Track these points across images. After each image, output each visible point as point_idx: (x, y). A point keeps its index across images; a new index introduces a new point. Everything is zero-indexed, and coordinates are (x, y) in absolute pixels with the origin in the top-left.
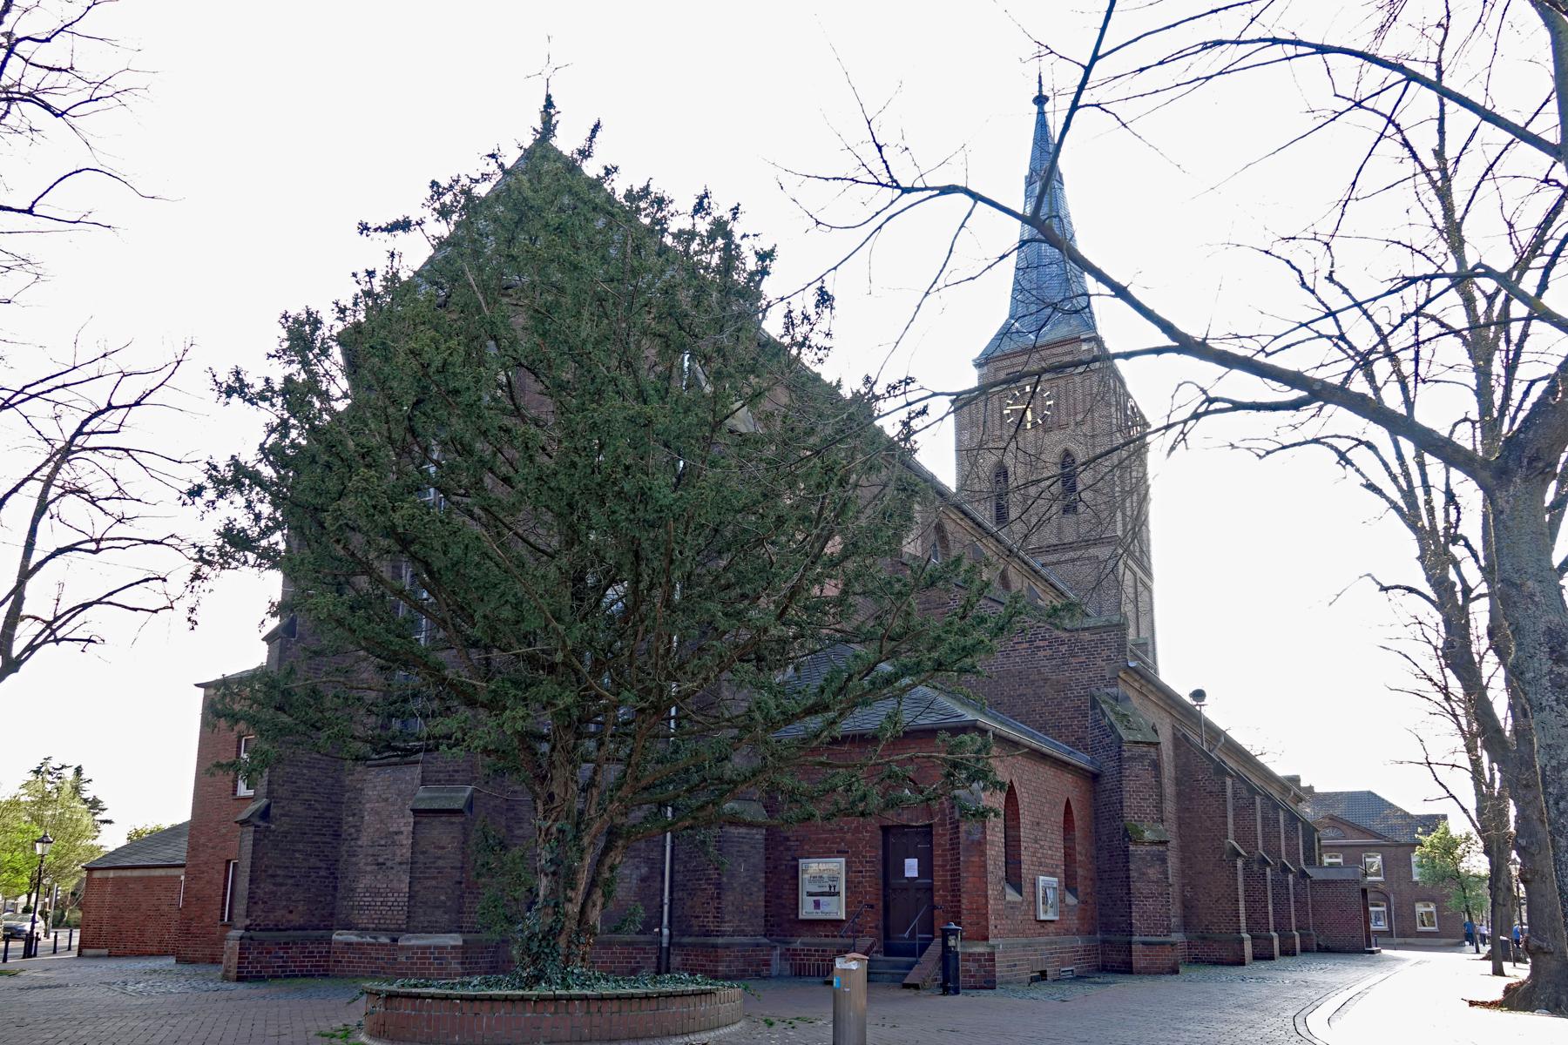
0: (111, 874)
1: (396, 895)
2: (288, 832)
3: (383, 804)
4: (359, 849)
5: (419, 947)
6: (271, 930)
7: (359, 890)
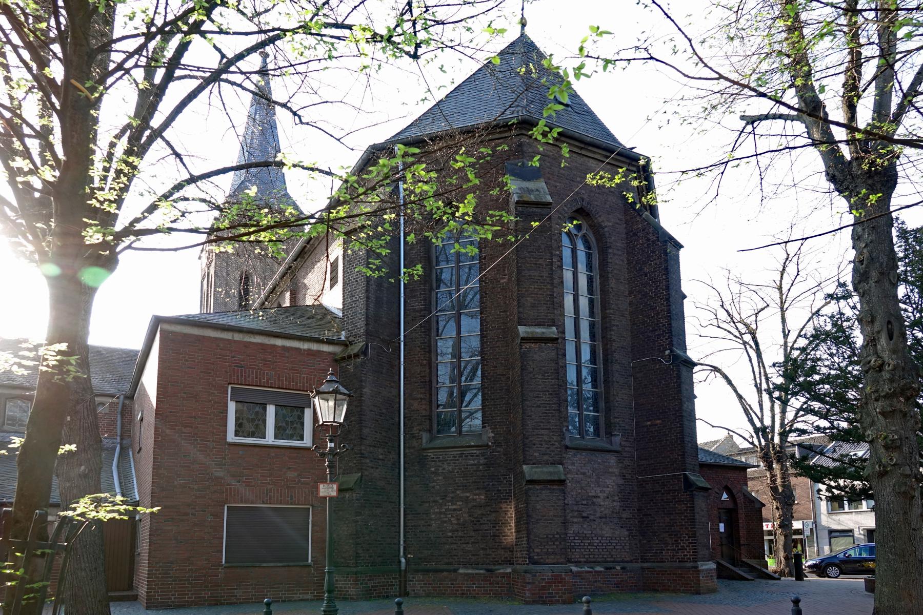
7: (569, 535)
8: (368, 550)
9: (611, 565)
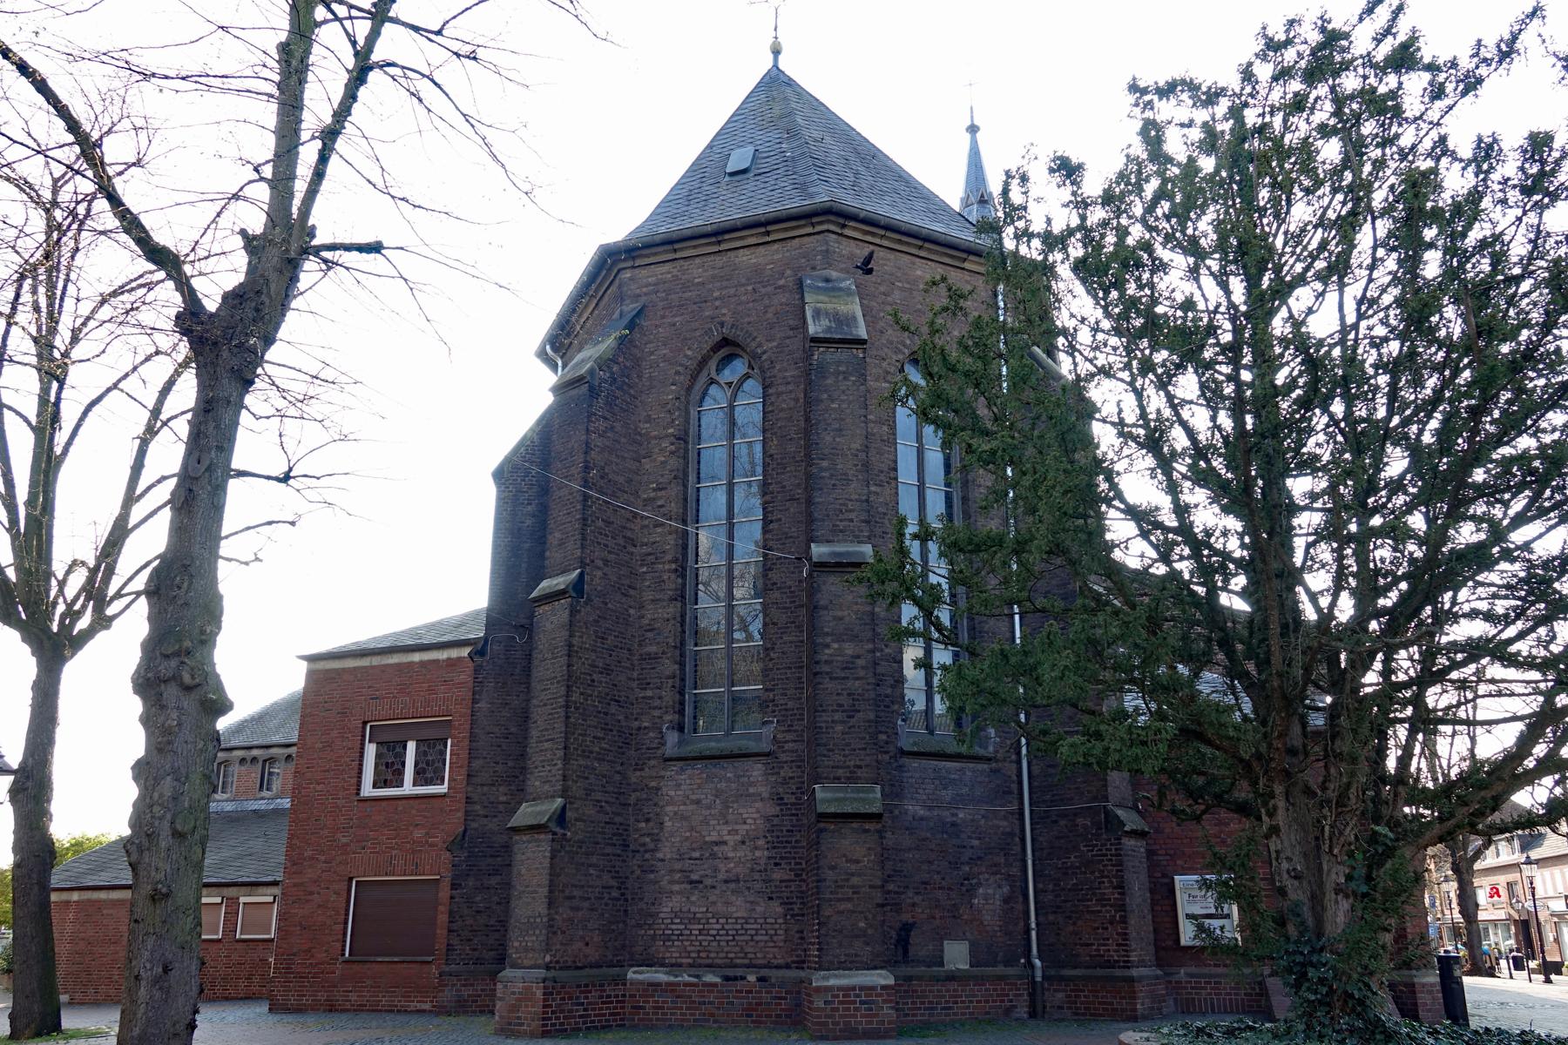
0: (75, 896)
1: (721, 921)
2: (583, 842)
3: (691, 807)
4: (660, 864)
5: (840, 988)
6: (568, 968)
7: (662, 915)
8: (470, 940)
9: (739, 972)
